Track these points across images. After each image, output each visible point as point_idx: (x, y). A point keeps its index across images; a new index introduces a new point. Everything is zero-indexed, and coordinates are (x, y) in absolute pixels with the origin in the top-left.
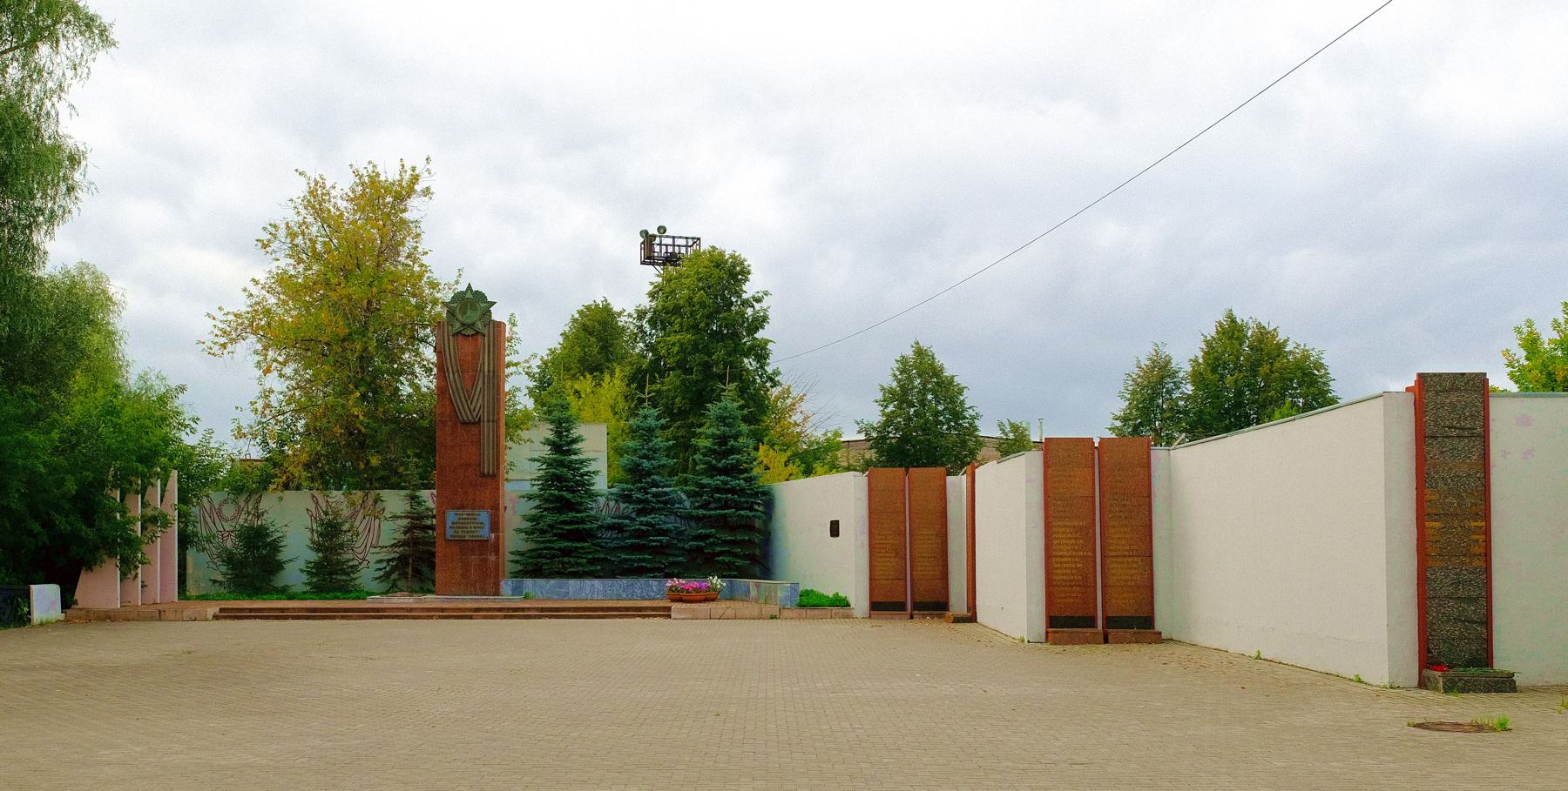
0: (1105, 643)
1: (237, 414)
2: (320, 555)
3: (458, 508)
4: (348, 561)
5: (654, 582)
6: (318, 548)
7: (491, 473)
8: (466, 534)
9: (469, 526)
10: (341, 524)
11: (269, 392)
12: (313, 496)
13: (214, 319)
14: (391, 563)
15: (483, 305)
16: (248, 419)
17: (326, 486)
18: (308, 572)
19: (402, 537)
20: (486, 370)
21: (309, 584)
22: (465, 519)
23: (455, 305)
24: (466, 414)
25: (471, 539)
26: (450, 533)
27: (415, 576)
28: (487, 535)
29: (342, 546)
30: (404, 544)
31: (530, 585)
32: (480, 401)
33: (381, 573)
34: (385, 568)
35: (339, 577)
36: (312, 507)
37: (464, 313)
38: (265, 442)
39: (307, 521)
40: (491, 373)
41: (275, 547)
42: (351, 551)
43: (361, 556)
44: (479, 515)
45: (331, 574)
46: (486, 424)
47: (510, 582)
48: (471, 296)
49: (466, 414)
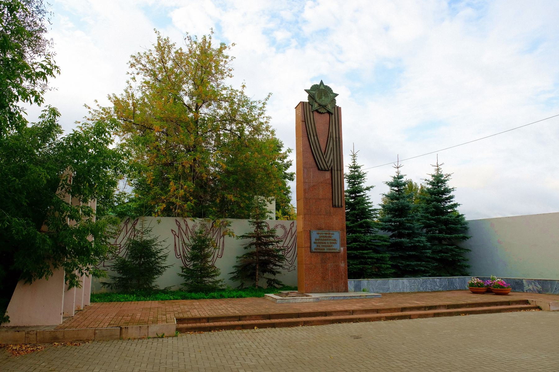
0: (92, 295)
12: (176, 221)
13: (89, 108)
15: (331, 95)
22: (323, 237)
23: (314, 92)
24: (324, 165)
25: (328, 251)
28: (338, 249)
31: (366, 284)
36: (176, 229)
37: (321, 98)
40: (337, 139)
44: (333, 234)
46: (336, 172)
47: (353, 282)
48: (324, 88)
49: (324, 165)
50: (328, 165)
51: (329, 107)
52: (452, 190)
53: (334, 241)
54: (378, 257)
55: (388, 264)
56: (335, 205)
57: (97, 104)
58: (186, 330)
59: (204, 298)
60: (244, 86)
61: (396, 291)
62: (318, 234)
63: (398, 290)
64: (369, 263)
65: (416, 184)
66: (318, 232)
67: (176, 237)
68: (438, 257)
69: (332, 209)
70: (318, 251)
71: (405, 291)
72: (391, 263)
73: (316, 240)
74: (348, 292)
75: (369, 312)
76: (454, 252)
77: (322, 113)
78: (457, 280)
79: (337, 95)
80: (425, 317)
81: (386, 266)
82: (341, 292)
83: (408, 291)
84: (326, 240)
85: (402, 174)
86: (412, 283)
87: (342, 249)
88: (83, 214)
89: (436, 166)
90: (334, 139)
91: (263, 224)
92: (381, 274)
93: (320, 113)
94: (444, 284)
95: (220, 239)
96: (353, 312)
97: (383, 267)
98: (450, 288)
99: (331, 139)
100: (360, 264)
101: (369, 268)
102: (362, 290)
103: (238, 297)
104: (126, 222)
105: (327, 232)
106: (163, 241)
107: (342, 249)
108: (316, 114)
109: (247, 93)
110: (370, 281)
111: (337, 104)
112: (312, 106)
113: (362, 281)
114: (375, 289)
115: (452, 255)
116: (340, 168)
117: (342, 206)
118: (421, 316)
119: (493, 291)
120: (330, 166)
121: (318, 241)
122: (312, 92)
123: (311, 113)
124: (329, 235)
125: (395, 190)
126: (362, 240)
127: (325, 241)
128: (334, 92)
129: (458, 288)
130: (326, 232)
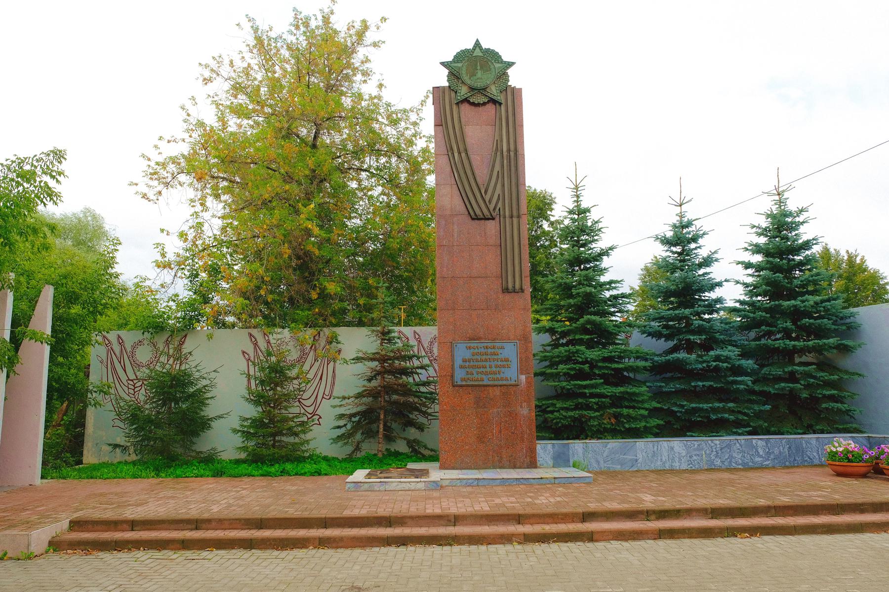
1: (162, 238)
2: (260, 409)
3: (472, 339)
4: (299, 415)
5: (760, 442)
6: (258, 400)
7: (517, 286)
8: (484, 376)
9: (488, 364)
11: (218, 323)
12: (251, 335)
13: (149, 160)
14: (353, 419)
15: (497, 65)
16: (175, 247)
17: (270, 322)
18: (244, 432)
20: (505, 149)
21: (244, 449)
23: (460, 65)
28: (514, 377)
29: (287, 397)
32: (499, 186)
33: (343, 430)
34: (345, 425)
35: (284, 439)
36: (250, 350)
37: (473, 74)
38: (194, 275)
39: (243, 364)
40: (512, 154)
41: (199, 399)
42: (297, 404)
43: (310, 410)
44: (502, 348)
45: (274, 435)
46: (508, 220)
47: (550, 447)
48: (481, 54)
50: (491, 207)
51: (494, 91)
52: (814, 242)
53: (504, 363)
54: (615, 393)
55: (643, 408)
56: (507, 289)
57: (158, 151)
58: (68, 545)
59: (249, 475)
60: (381, 86)
61: (653, 467)
62: (470, 348)
63: (658, 465)
64: (595, 407)
65: (837, 252)
66: (469, 345)
67: (250, 363)
68: (773, 392)
69: (501, 296)
71: (676, 465)
74: (536, 467)
75: (498, 520)
76: (812, 380)
77: (478, 105)
78: (814, 442)
79: (510, 64)
80: (634, 539)
82: (520, 468)
83: (684, 466)
84: (486, 360)
85: (689, 216)
86: (695, 450)
87: (523, 378)
89: (774, 194)
90: (505, 153)
91: (393, 335)
92: (623, 429)
93: (473, 104)
94: (776, 451)
95: (328, 364)
96: (456, 520)
98: (795, 460)
99: (499, 153)
100: (575, 409)
102: (571, 464)
103: (312, 474)
104: (167, 340)
105: (489, 345)
106: (214, 371)
107: (523, 378)
108: (465, 107)
109: (388, 96)
110: (590, 445)
111: (513, 82)
112: (456, 92)
113: (571, 445)
114: (602, 462)
115: (808, 386)
117: (522, 290)
118: (621, 536)
119: (885, 471)
120: (494, 209)
121: (468, 363)
122: (456, 65)
123: (455, 107)
124: (493, 351)
125: (676, 253)
126: (581, 358)
127: (484, 363)
128: (505, 58)
129: (816, 462)
130: (486, 344)
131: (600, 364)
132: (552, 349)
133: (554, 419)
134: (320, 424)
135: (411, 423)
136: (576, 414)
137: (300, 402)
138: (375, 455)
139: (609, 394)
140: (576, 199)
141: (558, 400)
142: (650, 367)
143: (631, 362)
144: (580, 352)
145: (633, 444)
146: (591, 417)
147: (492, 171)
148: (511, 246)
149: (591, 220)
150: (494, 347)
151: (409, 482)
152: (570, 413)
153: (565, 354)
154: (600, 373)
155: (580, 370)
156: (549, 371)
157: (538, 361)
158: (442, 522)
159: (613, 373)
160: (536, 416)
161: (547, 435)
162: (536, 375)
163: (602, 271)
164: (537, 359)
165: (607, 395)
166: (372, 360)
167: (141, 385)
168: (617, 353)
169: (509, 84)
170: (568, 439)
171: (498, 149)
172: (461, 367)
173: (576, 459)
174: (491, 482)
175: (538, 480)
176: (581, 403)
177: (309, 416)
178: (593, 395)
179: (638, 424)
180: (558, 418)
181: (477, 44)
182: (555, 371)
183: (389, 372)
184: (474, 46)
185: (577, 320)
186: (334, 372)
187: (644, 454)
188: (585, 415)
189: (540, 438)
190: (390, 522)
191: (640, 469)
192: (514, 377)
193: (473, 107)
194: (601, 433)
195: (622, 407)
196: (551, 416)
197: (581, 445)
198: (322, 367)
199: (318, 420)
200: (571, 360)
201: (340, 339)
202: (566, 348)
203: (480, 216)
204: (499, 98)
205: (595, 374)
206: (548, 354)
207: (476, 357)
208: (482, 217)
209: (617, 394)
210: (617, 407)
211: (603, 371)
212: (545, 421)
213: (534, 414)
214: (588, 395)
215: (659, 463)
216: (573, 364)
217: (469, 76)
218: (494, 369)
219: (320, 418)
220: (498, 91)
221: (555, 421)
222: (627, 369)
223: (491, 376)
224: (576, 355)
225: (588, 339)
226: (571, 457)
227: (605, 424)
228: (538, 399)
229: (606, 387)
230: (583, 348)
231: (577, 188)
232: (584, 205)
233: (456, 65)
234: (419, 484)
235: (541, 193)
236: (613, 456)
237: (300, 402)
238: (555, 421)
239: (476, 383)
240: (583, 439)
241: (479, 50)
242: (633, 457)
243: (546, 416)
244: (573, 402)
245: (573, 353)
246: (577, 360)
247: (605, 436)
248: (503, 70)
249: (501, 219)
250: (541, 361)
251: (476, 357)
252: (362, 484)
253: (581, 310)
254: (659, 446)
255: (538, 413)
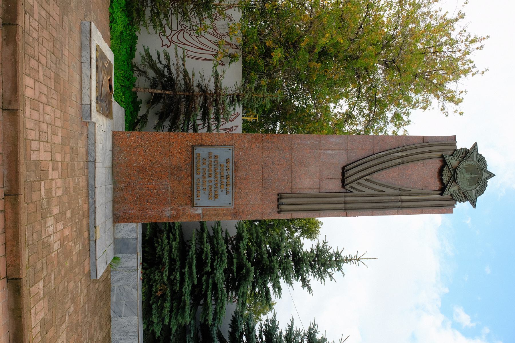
3: (236, 164)
7: (283, 207)
8: (201, 174)
9: (213, 179)
10: (210, 16)
14: (166, 70)
15: (474, 192)
19: (195, 83)
20: (403, 198)
23: (475, 159)
25: (195, 181)
26: (203, 152)
27: (152, 95)
28: (200, 203)
30: (188, 86)
33: (155, 57)
34: (160, 62)
37: (467, 171)
40: (399, 204)
42: (180, 28)
43: (175, 39)
44: (227, 193)
46: (343, 199)
47: (134, 235)
50: (354, 185)
51: (453, 188)
53: (213, 194)
54: (184, 295)
55: (170, 319)
56: (281, 198)
61: (114, 331)
64: (172, 277)
69: (275, 192)
70: (195, 161)
72: (174, 329)
73: (216, 157)
81: (166, 312)
82: (114, 207)
84: (216, 177)
87: (199, 211)
88: (222, 239)
90: (400, 198)
92: (151, 302)
95: (212, 55)
97: (165, 305)
99: (400, 192)
101: (162, 275)
105: (230, 180)
108: (437, 164)
110: (135, 273)
112: (452, 155)
113: (135, 256)
116: (352, 209)
117: (279, 212)
120: (352, 187)
122: (475, 156)
123: (440, 154)
124: (225, 183)
126: (217, 264)
127: (213, 175)
128: (479, 199)
130: (231, 177)
131: (211, 281)
132: (223, 238)
133: (162, 240)
134: (162, 46)
135: (162, 117)
136: (166, 259)
137: (181, 30)
138: (134, 85)
139: (183, 290)
140: (349, 258)
141: (179, 243)
142: (208, 324)
143: (212, 308)
144: (221, 263)
145: (136, 313)
146: (162, 273)
147: (385, 186)
148: (319, 202)
149: (333, 272)
150: (228, 185)
151: (90, 88)
152: (166, 254)
153: (220, 250)
154: (203, 281)
155: (206, 263)
156: (205, 235)
157: (213, 226)
158: (8, 93)
159: (203, 293)
160: (165, 223)
161: (148, 233)
162: (202, 223)
163: (288, 280)
164: (215, 225)
165: (182, 288)
166: (216, 86)
167: (197, 23)
168: (220, 296)
169: (458, 202)
170: (143, 252)
171: (403, 191)
172: (210, 154)
173: (123, 260)
174: (92, 175)
175: (93, 223)
176: (176, 264)
177: (169, 38)
178: (182, 275)
179: (155, 316)
180: (162, 243)
181: (491, 175)
182: (205, 241)
183: (206, 99)
184: (489, 172)
185: (250, 261)
186: (206, 59)
187: (127, 323)
188: (165, 268)
189: (144, 226)
190: (9, 24)
191: (112, 320)
192: (200, 203)
193: (437, 170)
194: (148, 282)
195: (172, 300)
196: (164, 237)
197: (136, 265)
198: (211, 50)
199: (166, 45)
200: (214, 256)
201: (233, 64)
202: (225, 251)
203: (347, 174)
204: (447, 193)
205: (202, 276)
206: (220, 234)
207: (219, 168)
208: (346, 176)
209: (183, 298)
210: (172, 296)
211: (204, 283)
212: (161, 232)
213: (165, 221)
214: (183, 271)
215: (118, 337)
216: (211, 257)
217: (465, 167)
218: (208, 184)
219: (168, 47)
220: (452, 192)
221: (160, 240)
222: (206, 304)
223: (201, 183)
224: (219, 260)
225: (233, 269)
226: (124, 255)
227: (156, 286)
228: (180, 226)
229: (190, 286)
230: (225, 265)
231: (358, 260)
232: (344, 266)
233: (475, 156)
234: (88, 98)
235: (318, 231)
236: (124, 294)
237: (181, 30)
238: (160, 240)
239: (195, 167)
240: (143, 265)
241: (486, 176)
242: (123, 312)
243: (165, 233)
244: (176, 257)
245: (221, 257)
246: (214, 262)
247: (145, 286)
248: (469, 197)
249: (344, 194)
250: (214, 229)
251: (219, 168)
252: (88, 39)
253: (258, 264)
254: (134, 337)
255: (168, 225)
